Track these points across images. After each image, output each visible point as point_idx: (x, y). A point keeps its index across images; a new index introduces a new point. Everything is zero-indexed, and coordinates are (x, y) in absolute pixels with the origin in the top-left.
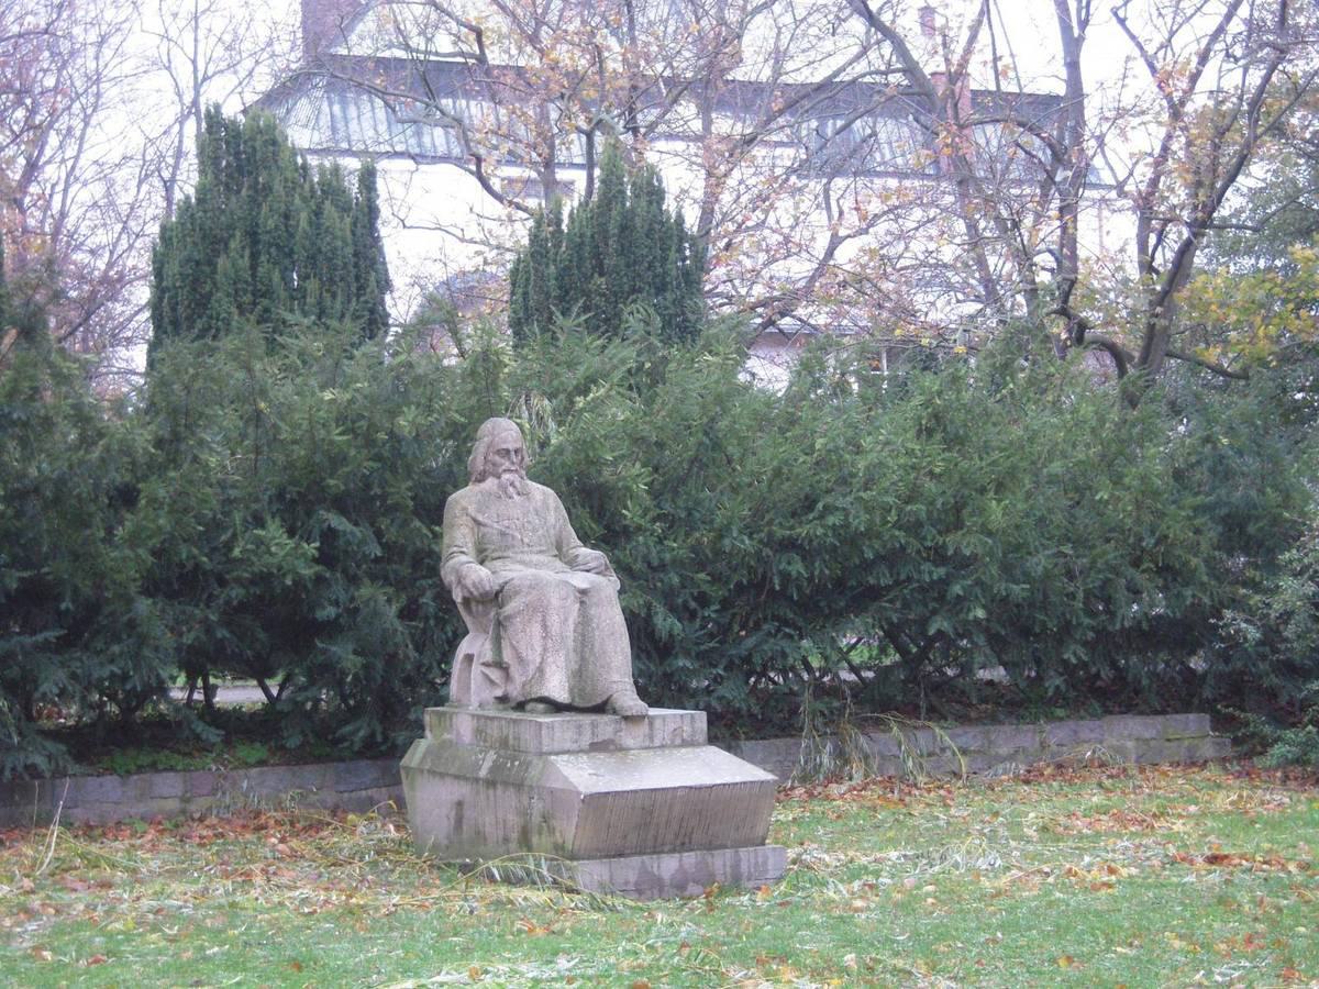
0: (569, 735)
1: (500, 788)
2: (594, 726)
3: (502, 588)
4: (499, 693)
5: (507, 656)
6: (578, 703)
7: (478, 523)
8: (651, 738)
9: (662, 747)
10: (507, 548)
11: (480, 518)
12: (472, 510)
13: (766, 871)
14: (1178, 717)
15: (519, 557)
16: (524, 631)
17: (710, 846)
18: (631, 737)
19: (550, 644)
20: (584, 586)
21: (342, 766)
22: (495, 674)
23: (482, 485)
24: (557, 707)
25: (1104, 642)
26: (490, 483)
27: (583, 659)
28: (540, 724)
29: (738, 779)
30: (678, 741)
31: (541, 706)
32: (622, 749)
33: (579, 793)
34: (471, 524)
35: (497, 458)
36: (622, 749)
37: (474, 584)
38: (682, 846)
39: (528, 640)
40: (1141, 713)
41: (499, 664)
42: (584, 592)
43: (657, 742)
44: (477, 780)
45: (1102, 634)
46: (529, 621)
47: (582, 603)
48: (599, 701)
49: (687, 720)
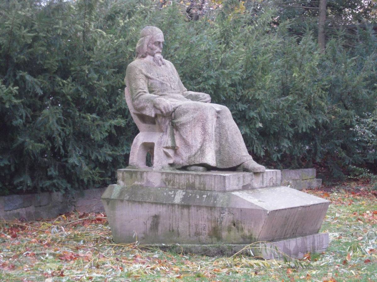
0: (236, 182)
1: (193, 210)
2: (244, 177)
3: (175, 110)
4: (171, 161)
5: (178, 143)
6: (219, 166)
7: (148, 78)
8: (263, 183)
9: (266, 187)
10: (165, 90)
11: (149, 75)
12: (144, 71)
13: (323, 245)
14: (306, 170)
15: (171, 94)
16: (191, 131)
17: (303, 235)
18: (256, 182)
19: (207, 137)
20: (218, 109)
21: (6, 198)
22: (171, 152)
23: (145, 59)
24: (208, 168)
25: (300, 137)
26: (149, 58)
27: (221, 145)
28: (224, 177)
29: (312, 203)
30: (272, 184)
31: (201, 168)
32: (253, 189)
33: (266, 211)
34: (144, 78)
35: (154, 46)
36: (253, 189)
37: (164, 108)
38: (293, 236)
39: (194, 136)
40: (293, 169)
41: (174, 148)
42: (218, 112)
43: (265, 185)
44: (173, 205)
45: (296, 134)
46: (194, 126)
47: (218, 117)
48: (234, 165)
49: (275, 174)
